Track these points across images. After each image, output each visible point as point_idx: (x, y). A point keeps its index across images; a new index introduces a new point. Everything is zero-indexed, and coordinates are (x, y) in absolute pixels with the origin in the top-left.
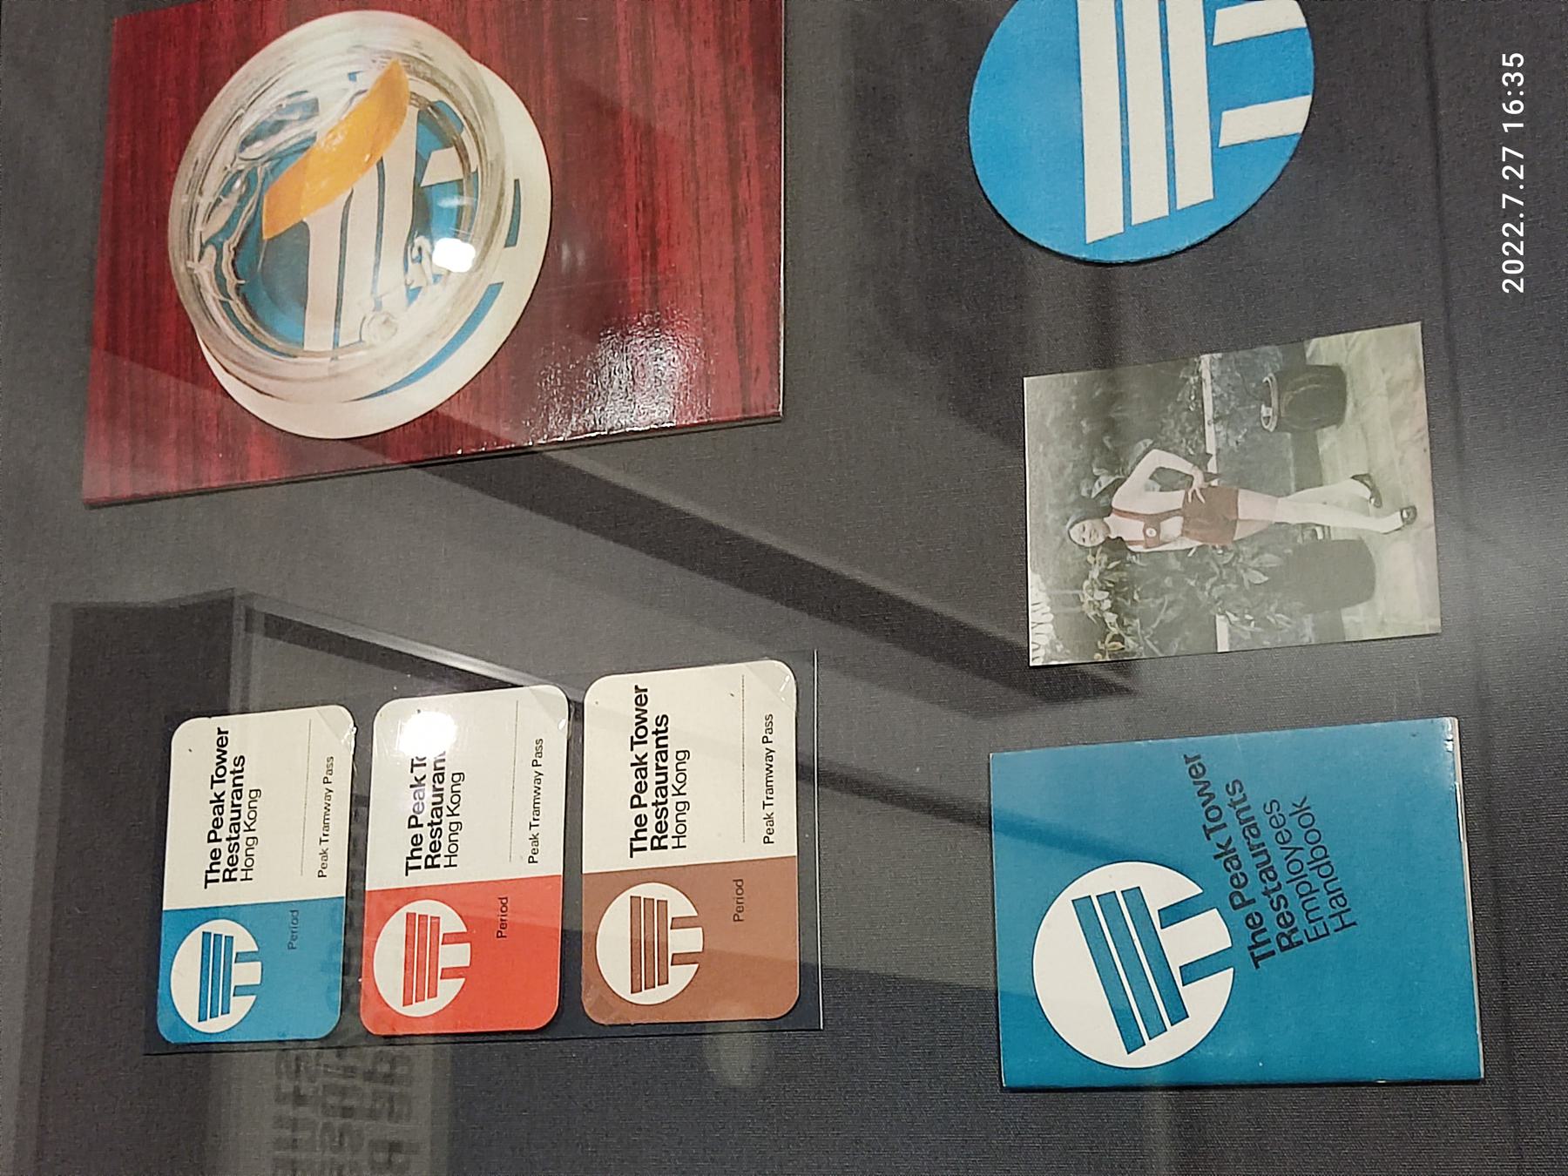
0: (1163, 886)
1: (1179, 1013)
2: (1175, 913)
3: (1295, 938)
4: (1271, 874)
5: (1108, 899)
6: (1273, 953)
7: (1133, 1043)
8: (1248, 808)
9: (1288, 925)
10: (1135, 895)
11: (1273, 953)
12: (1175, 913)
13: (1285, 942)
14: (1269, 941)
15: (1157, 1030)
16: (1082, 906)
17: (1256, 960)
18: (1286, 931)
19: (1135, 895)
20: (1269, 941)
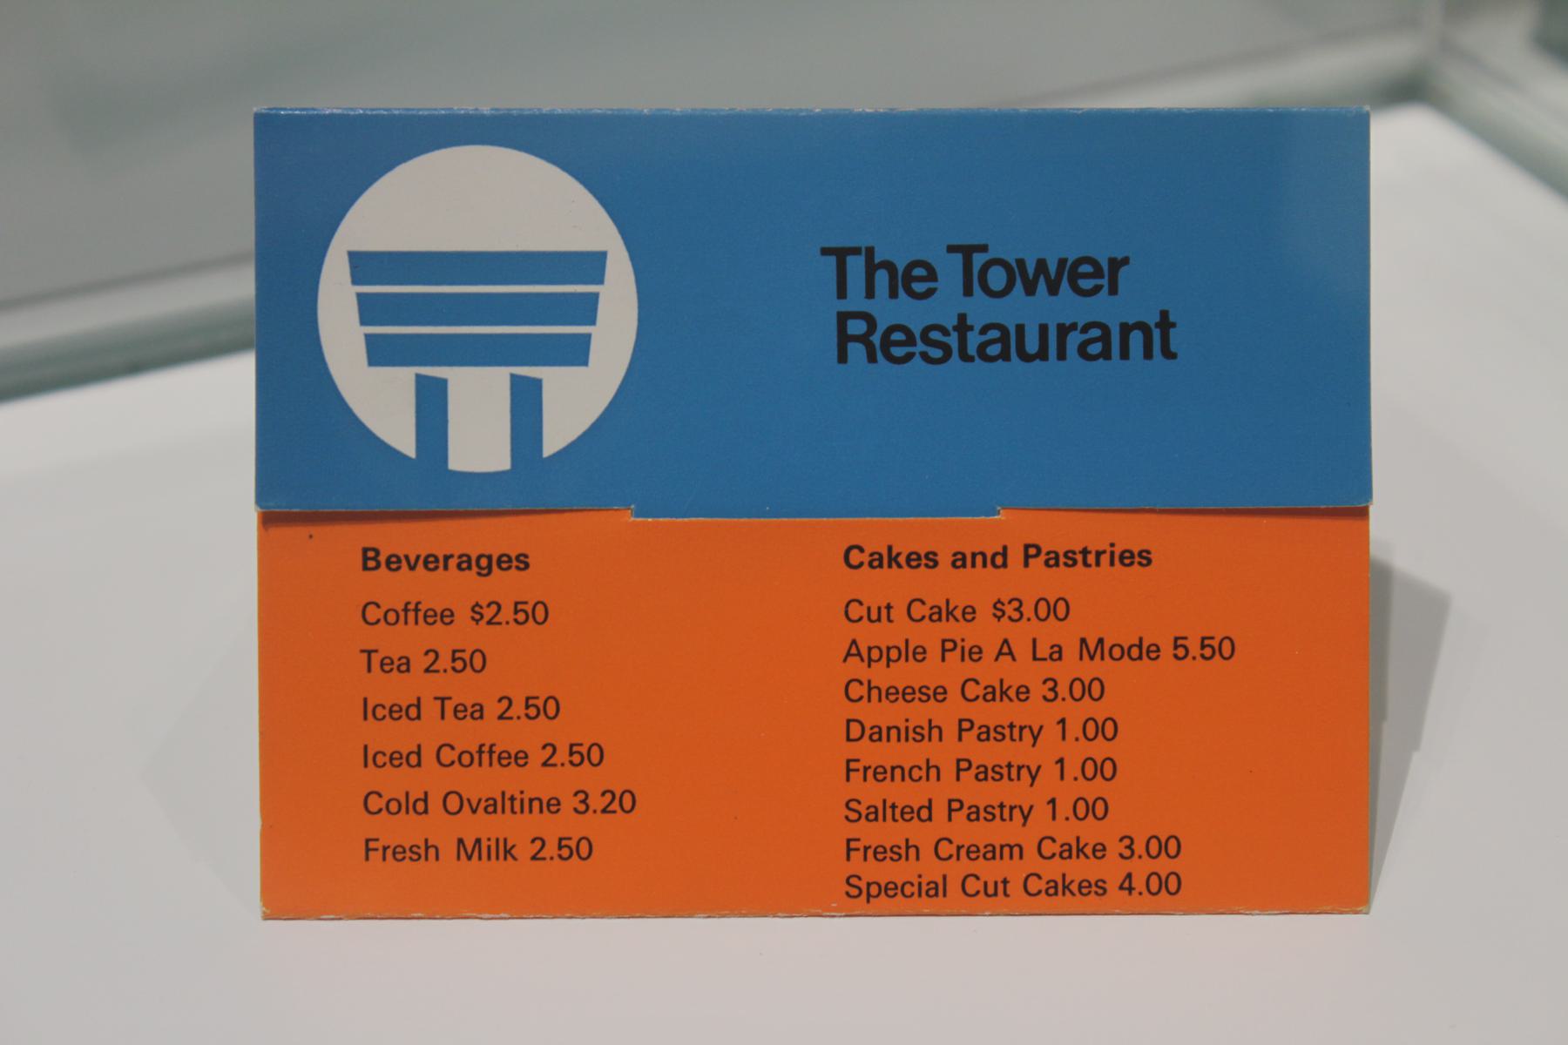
0: (575, 402)
1: (380, 353)
2: (527, 404)
3: (856, 351)
4: (994, 350)
5: (586, 309)
6: (842, 293)
7: (364, 265)
8: (1148, 354)
9: (887, 343)
10: (575, 352)
11: (842, 293)
12: (527, 404)
13: (856, 327)
14: (870, 294)
15: (370, 310)
16: (591, 265)
17: (841, 255)
18: (876, 339)
19: (575, 352)
20: (870, 294)
